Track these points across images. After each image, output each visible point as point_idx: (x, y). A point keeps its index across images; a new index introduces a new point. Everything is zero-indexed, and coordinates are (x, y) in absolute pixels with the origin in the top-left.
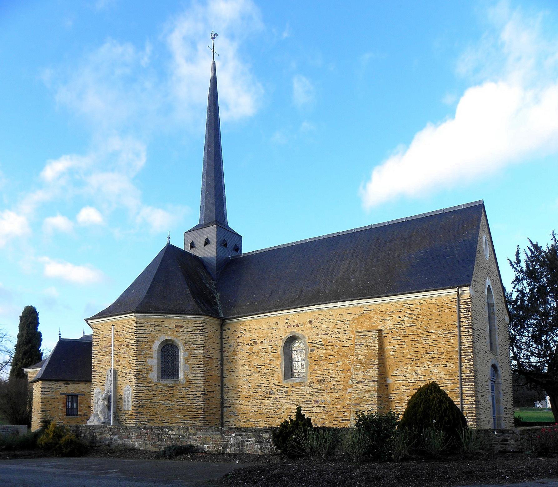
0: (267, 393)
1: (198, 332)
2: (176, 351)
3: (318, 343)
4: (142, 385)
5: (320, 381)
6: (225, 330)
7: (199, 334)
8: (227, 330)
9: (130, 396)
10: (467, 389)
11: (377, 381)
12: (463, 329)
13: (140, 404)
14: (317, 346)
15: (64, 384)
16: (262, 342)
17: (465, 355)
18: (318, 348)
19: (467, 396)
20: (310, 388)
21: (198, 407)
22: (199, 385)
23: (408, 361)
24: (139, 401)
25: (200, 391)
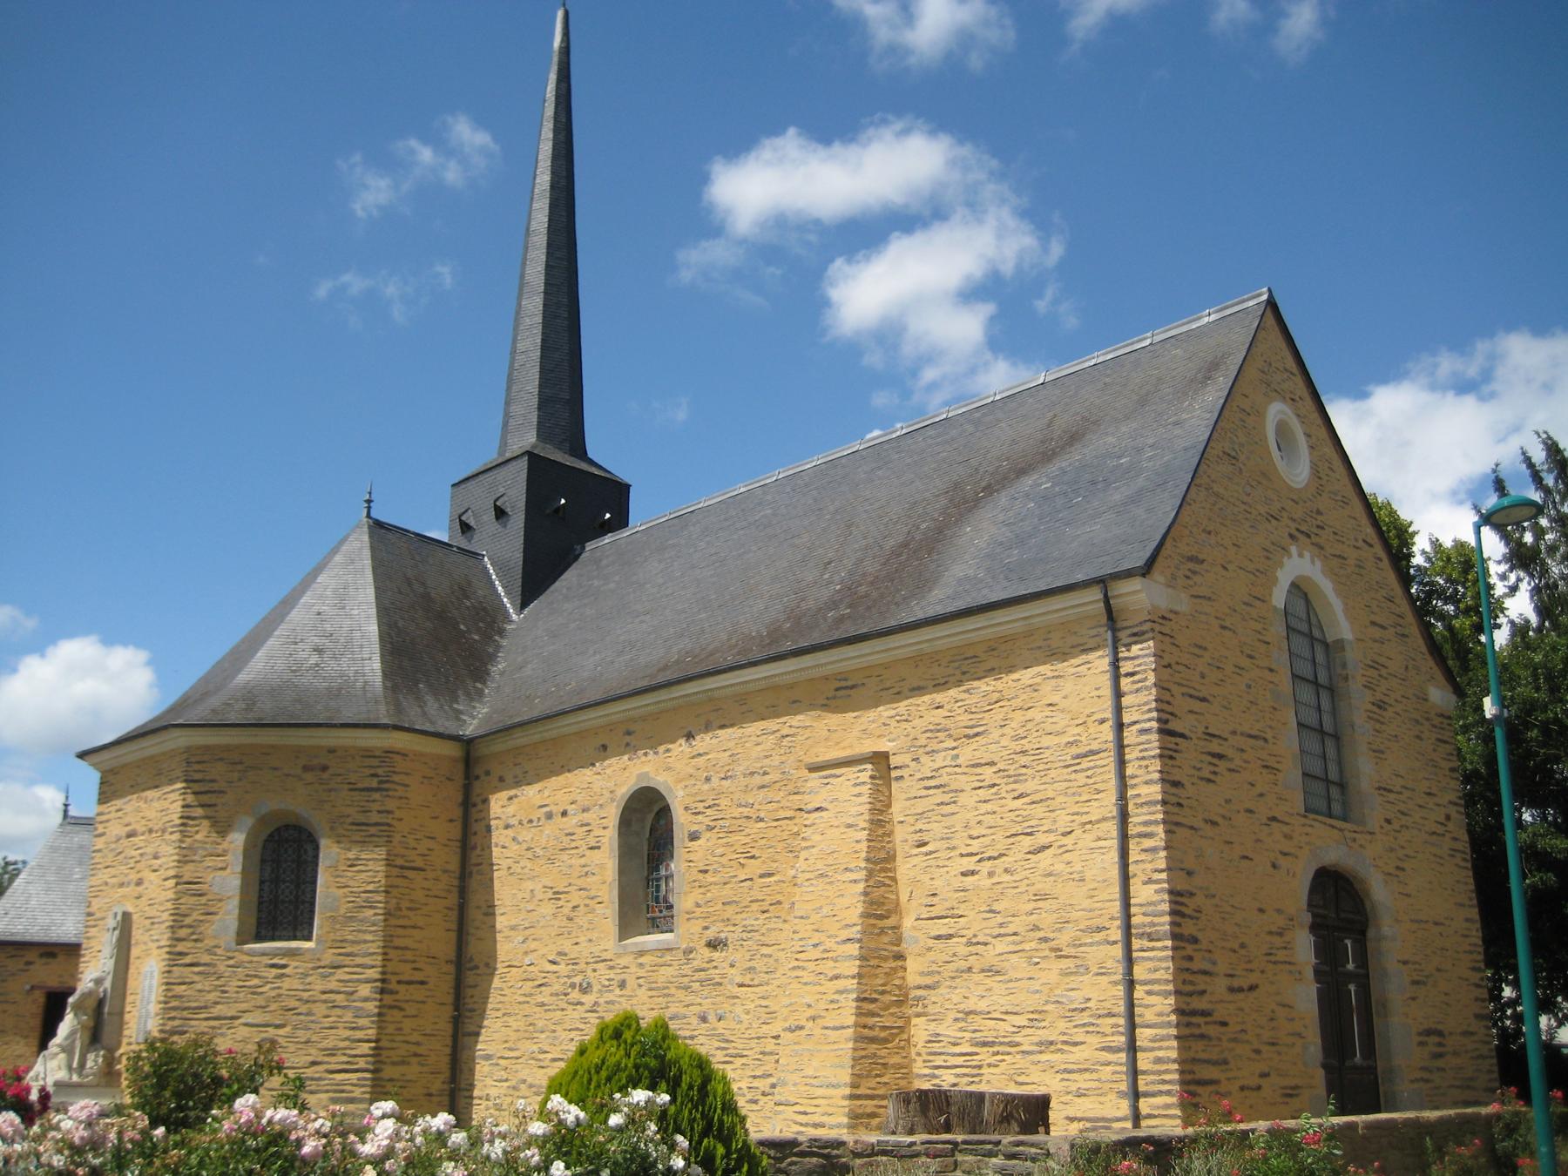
0: (573, 986)
1: (374, 784)
2: (309, 847)
3: (709, 812)
4: (188, 960)
5: (713, 945)
6: (477, 778)
7: (377, 790)
8: (483, 777)
9: (153, 998)
10: (1150, 964)
11: (859, 941)
12: (1130, 736)
13: (177, 1023)
14: (707, 821)
15: (42, 955)
16: (564, 814)
17: (1140, 835)
18: (710, 829)
19: (1149, 993)
20: (687, 970)
21: (359, 1034)
22: (368, 961)
23: (968, 864)
24: (173, 1014)
25: (367, 981)
